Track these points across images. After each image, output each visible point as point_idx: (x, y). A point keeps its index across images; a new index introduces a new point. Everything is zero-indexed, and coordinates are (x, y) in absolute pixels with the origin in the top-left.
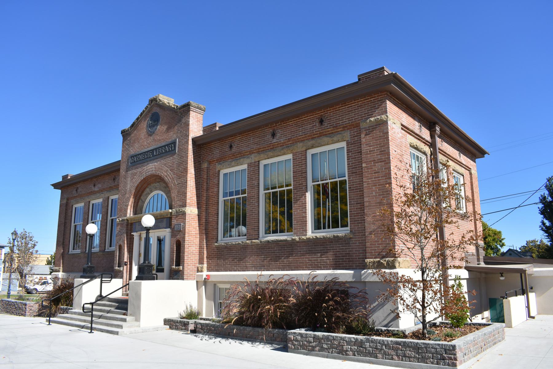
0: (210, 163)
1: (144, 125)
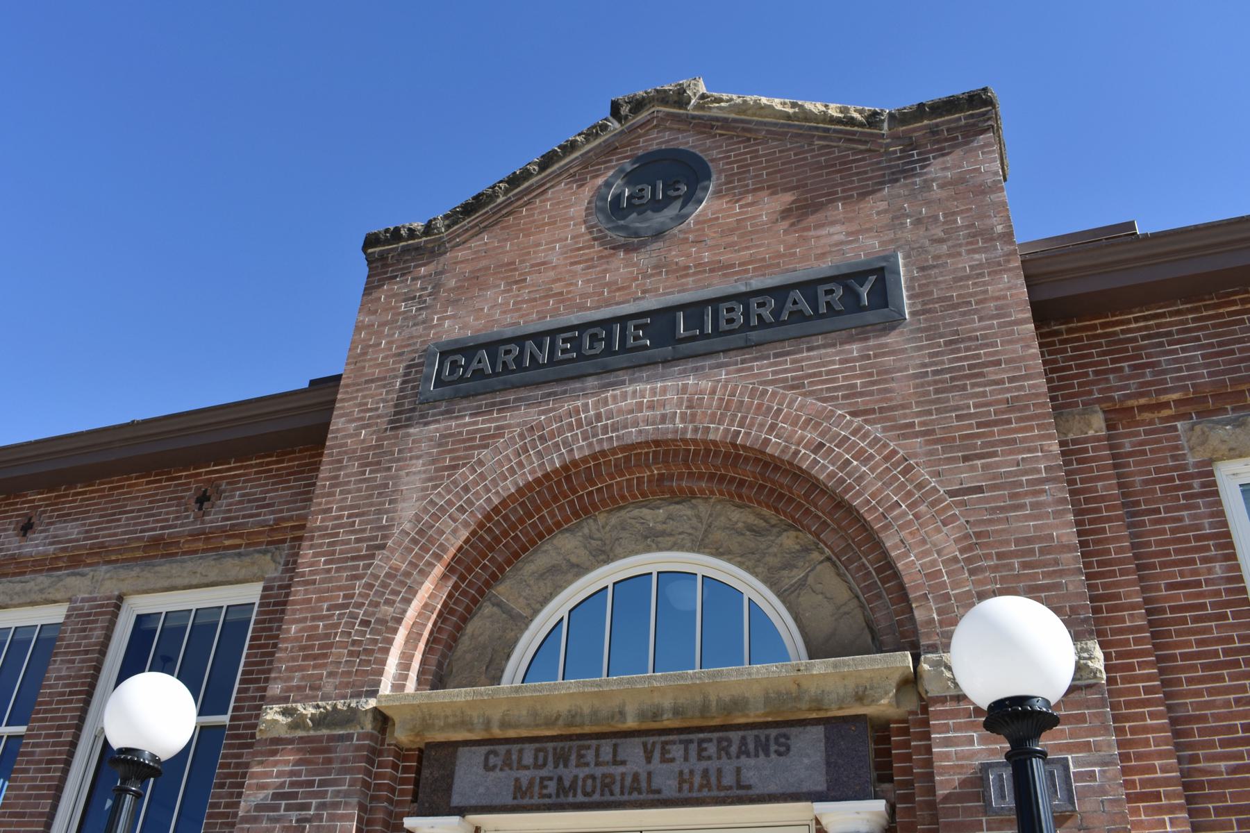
0: (1117, 416)
1: (570, 206)
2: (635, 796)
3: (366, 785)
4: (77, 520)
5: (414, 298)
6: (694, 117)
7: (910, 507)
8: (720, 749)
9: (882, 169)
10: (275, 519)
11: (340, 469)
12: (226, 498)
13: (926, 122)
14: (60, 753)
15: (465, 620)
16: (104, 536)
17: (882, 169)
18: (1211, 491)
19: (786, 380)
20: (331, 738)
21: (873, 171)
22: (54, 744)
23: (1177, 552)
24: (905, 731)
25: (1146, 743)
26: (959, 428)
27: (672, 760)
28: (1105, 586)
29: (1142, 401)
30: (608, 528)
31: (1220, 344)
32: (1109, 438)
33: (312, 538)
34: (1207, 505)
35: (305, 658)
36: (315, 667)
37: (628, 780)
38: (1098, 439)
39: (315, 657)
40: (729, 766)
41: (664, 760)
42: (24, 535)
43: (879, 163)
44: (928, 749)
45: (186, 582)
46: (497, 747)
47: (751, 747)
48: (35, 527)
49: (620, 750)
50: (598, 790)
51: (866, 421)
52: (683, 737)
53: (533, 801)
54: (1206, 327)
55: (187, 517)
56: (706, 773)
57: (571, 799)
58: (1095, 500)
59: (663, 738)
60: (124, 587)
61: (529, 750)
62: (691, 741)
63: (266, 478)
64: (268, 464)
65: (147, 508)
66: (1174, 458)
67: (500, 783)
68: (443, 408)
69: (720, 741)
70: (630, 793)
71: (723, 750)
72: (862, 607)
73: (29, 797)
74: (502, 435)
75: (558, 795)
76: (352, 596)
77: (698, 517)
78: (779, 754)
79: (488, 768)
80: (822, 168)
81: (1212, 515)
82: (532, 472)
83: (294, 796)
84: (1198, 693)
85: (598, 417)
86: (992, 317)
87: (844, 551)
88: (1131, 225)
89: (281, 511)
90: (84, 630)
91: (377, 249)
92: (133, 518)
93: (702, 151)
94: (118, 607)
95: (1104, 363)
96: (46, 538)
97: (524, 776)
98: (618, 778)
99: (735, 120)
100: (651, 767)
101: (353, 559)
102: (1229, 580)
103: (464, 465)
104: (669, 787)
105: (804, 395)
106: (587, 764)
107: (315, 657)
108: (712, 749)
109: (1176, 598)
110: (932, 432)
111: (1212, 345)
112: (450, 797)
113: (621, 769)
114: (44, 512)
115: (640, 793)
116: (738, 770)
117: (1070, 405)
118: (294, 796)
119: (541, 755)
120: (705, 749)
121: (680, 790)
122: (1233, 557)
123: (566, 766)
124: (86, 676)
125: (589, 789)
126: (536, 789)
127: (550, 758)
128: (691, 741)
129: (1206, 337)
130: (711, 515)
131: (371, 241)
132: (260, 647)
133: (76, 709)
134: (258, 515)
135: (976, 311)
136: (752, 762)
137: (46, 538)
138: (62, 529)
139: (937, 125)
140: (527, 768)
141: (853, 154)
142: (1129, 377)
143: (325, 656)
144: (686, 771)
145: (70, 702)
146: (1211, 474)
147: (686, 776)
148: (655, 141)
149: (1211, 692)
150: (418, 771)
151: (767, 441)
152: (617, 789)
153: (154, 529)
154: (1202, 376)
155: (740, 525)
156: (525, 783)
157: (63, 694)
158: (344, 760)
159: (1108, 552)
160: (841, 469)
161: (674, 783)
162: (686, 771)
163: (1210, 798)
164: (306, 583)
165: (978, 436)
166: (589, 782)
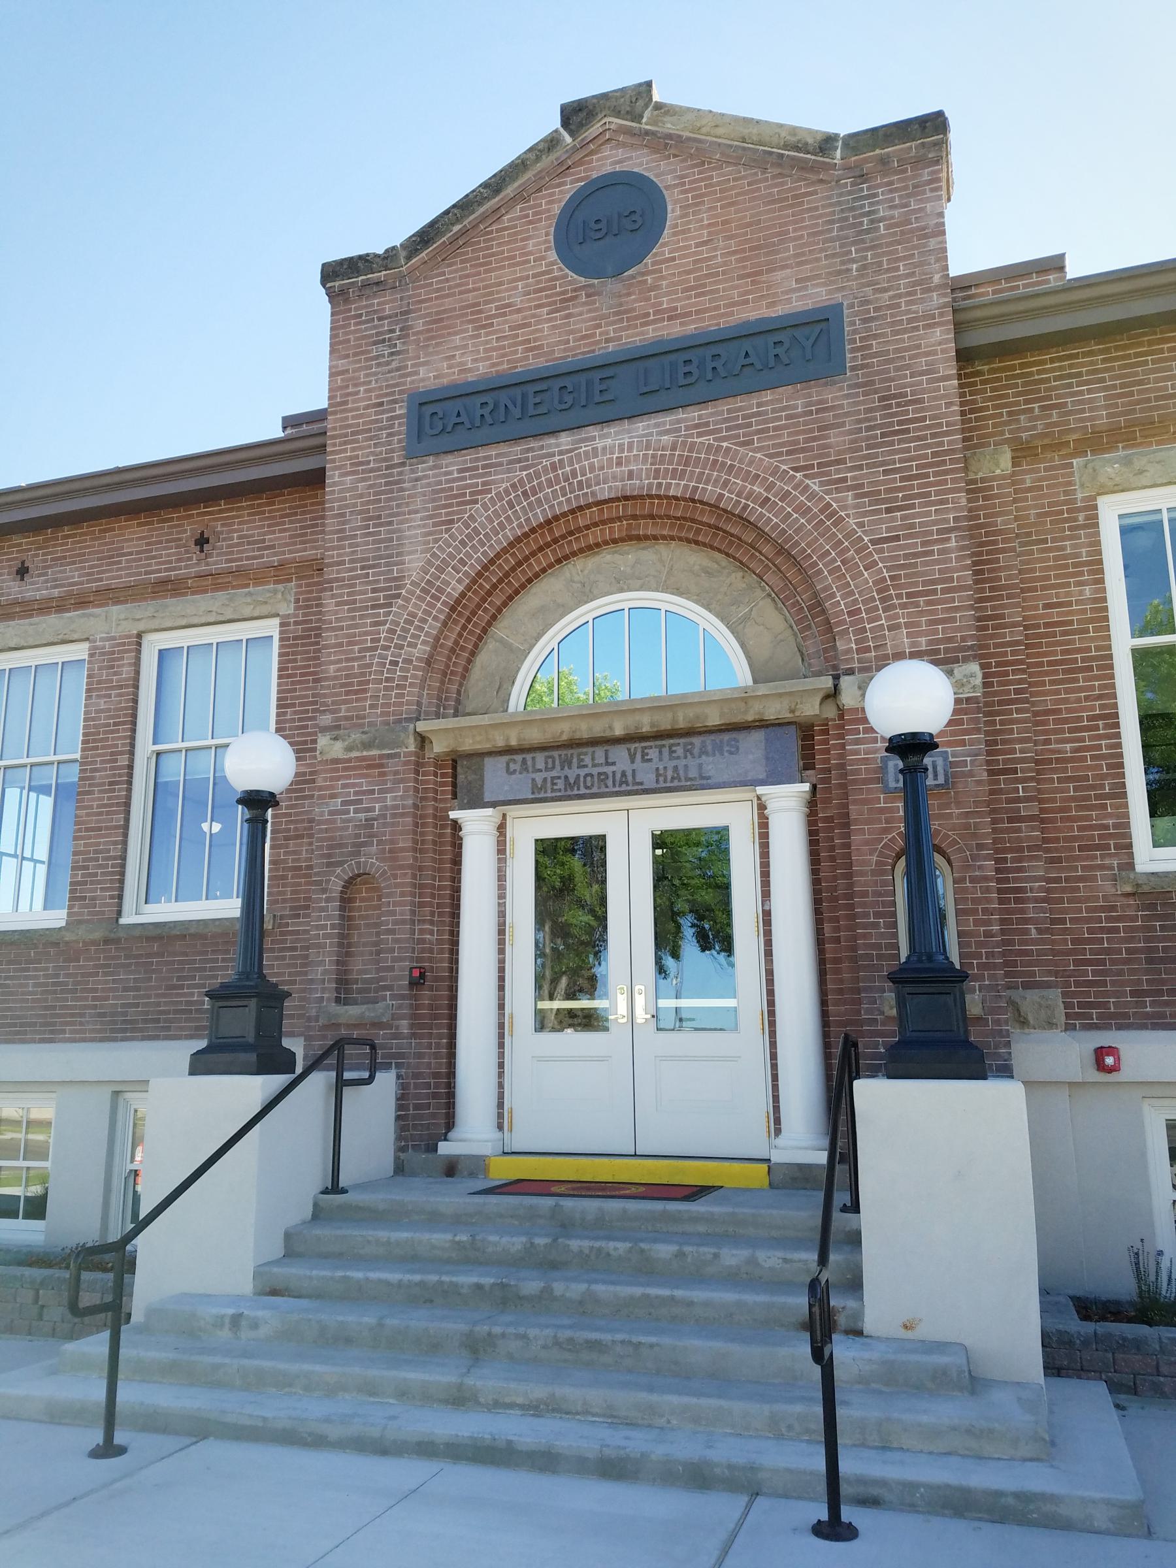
0: (1023, 452)
1: (533, 240)
2: (624, 787)
3: (416, 790)
4: (74, 563)
5: (384, 341)
6: (647, 133)
7: (839, 554)
8: (686, 751)
9: (831, 205)
10: (278, 561)
11: (344, 523)
12: (224, 540)
13: (878, 152)
14: (120, 775)
15: (473, 654)
16: (108, 579)
17: (831, 205)
18: (1093, 523)
19: (738, 436)
20: (381, 757)
21: (824, 207)
22: (112, 768)
23: (1057, 577)
24: (826, 732)
25: (1011, 731)
26: (884, 482)
27: (650, 760)
28: (993, 608)
29: (1047, 441)
30: (586, 572)
31: (1122, 386)
32: (1014, 474)
33: (331, 589)
34: (1087, 536)
35: (347, 693)
36: (357, 700)
37: (618, 776)
38: (1003, 477)
39: (357, 692)
40: (692, 763)
41: (644, 760)
42: (22, 580)
43: (829, 197)
44: (843, 746)
45: (203, 620)
46: (515, 757)
47: (709, 748)
48: (31, 572)
49: (610, 755)
50: (596, 784)
51: (805, 476)
52: (659, 743)
53: (629, 788)
54: (1112, 369)
55: (190, 559)
56: (676, 768)
57: (575, 792)
58: (994, 533)
59: (644, 744)
60: (141, 626)
61: (540, 758)
62: (664, 746)
63: (260, 520)
64: (259, 506)
65: (140, 549)
66: (1066, 493)
67: (521, 784)
68: (431, 463)
69: (685, 745)
70: (620, 786)
71: (688, 751)
72: (795, 635)
73: (101, 814)
74: (489, 491)
75: (566, 790)
76: (379, 640)
77: (661, 561)
78: (731, 753)
79: (510, 772)
80: (773, 202)
81: (1091, 544)
82: (520, 526)
83: (360, 802)
84: (1058, 692)
85: (574, 473)
86: (922, 373)
87: (782, 590)
88: (1056, 264)
89: (284, 553)
90: (112, 667)
91: (337, 284)
92: (135, 560)
93: (657, 176)
94: (139, 644)
95: (1017, 403)
96: (46, 581)
97: (539, 777)
98: (611, 775)
99: (689, 139)
100: (635, 766)
101: (374, 607)
102: (1095, 601)
103: (459, 520)
104: (649, 780)
105: (754, 451)
106: (586, 766)
107: (357, 692)
108: (680, 751)
109: (1050, 615)
110: (862, 486)
111: (1114, 387)
112: (483, 794)
113: (613, 768)
114: (37, 555)
115: (628, 785)
116: (700, 766)
117: (982, 445)
118: (360, 802)
119: (550, 761)
120: (675, 752)
121: (657, 781)
122: (1102, 581)
123: (570, 768)
124: (126, 708)
125: (589, 784)
126: (549, 785)
127: (557, 762)
128: (664, 746)
129: (1112, 378)
130: (671, 559)
131: (331, 273)
132: (289, 676)
133: (125, 738)
134: (262, 556)
135: (908, 367)
136: (711, 759)
137: (46, 581)
138: (60, 572)
139: (888, 154)
140: (540, 771)
141: (807, 186)
142: (1037, 418)
143: (365, 691)
144: (661, 767)
145: (118, 731)
146: (1095, 507)
147: (661, 772)
148: (609, 161)
149: (1067, 691)
150: (455, 776)
151: (721, 496)
152: (610, 782)
153: (159, 571)
154: (1101, 417)
155: (697, 567)
156: (539, 783)
157: (108, 725)
158: (396, 773)
159: (999, 579)
160: (783, 521)
161: (653, 776)
162: (661, 767)
163: (1054, 771)
164: (334, 629)
165: (900, 489)
166: (589, 779)
